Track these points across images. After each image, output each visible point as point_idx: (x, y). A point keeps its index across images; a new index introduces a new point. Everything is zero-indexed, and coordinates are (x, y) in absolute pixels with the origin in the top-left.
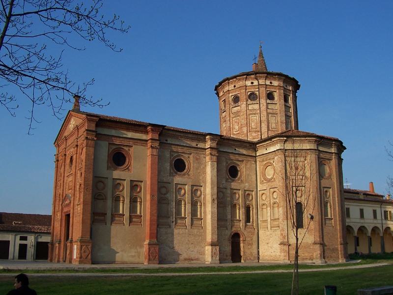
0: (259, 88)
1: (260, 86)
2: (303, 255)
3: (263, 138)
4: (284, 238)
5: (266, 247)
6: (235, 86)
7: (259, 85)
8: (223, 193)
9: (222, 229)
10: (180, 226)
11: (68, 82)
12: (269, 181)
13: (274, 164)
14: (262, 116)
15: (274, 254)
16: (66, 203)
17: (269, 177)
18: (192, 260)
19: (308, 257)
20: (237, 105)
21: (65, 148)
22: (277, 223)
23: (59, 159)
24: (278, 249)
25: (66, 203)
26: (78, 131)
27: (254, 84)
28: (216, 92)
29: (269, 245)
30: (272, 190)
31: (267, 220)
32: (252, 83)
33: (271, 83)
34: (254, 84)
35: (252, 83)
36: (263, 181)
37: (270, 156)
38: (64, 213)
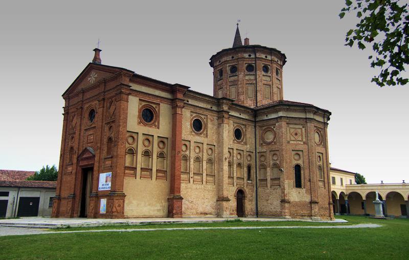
0: (255, 61)
1: (257, 59)
2: (302, 212)
3: (258, 105)
4: (282, 197)
5: (265, 203)
6: (233, 57)
7: (256, 58)
8: (319, 145)
10: (197, 181)
11: (356, 42)
12: (269, 144)
13: (275, 129)
14: (258, 86)
15: (274, 210)
16: (84, 156)
17: (268, 141)
18: (207, 214)
19: (306, 215)
20: (234, 74)
21: (82, 101)
22: (278, 182)
23: (70, 111)
24: (320, 199)
25: (84, 156)
26: (105, 85)
27: (251, 57)
28: (286, 60)
29: (269, 202)
30: (273, 153)
31: (267, 179)
32: (250, 56)
33: (266, 57)
34: (251, 57)
35: (250, 56)
36: (262, 144)
37: (272, 122)
38: (81, 166)
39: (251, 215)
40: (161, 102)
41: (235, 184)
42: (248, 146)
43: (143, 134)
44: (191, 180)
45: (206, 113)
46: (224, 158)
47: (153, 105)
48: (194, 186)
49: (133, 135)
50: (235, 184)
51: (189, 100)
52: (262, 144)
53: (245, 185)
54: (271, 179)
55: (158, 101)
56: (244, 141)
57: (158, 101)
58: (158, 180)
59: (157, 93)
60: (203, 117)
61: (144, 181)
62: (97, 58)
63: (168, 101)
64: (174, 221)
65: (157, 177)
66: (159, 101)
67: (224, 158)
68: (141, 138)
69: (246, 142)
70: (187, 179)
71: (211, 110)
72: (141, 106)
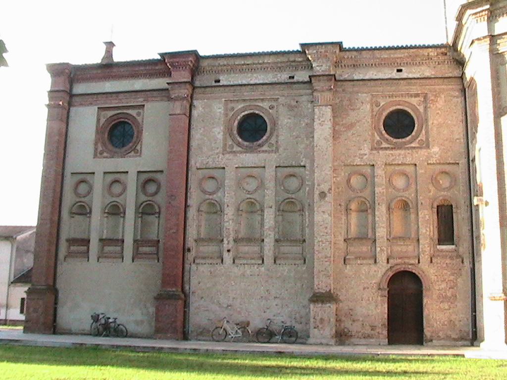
9: (359, 262)
39: (448, 337)
40: (147, 101)
41: (382, 258)
42: (435, 149)
43: (72, 173)
44: (227, 257)
45: (276, 92)
46: (317, 193)
47: (130, 112)
48: (236, 270)
49: (214, 175)
50: (382, 258)
51: (221, 78)
52: (379, 143)
53: (425, 258)
54: (101, 240)
55: (139, 101)
56: (422, 137)
57: (139, 101)
58: (138, 262)
59: (139, 84)
60: (414, 101)
61: (106, 264)
62: (109, 53)
63: (305, 85)
64: (145, 345)
65: (136, 256)
66: (141, 100)
67: (317, 193)
68: (98, 183)
69: (427, 139)
70: (118, 255)
71: (291, 83)
72: (103, 120)
